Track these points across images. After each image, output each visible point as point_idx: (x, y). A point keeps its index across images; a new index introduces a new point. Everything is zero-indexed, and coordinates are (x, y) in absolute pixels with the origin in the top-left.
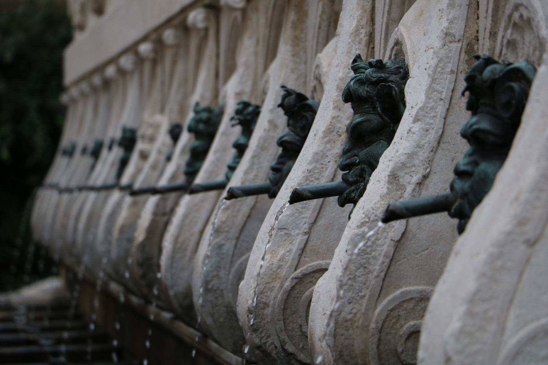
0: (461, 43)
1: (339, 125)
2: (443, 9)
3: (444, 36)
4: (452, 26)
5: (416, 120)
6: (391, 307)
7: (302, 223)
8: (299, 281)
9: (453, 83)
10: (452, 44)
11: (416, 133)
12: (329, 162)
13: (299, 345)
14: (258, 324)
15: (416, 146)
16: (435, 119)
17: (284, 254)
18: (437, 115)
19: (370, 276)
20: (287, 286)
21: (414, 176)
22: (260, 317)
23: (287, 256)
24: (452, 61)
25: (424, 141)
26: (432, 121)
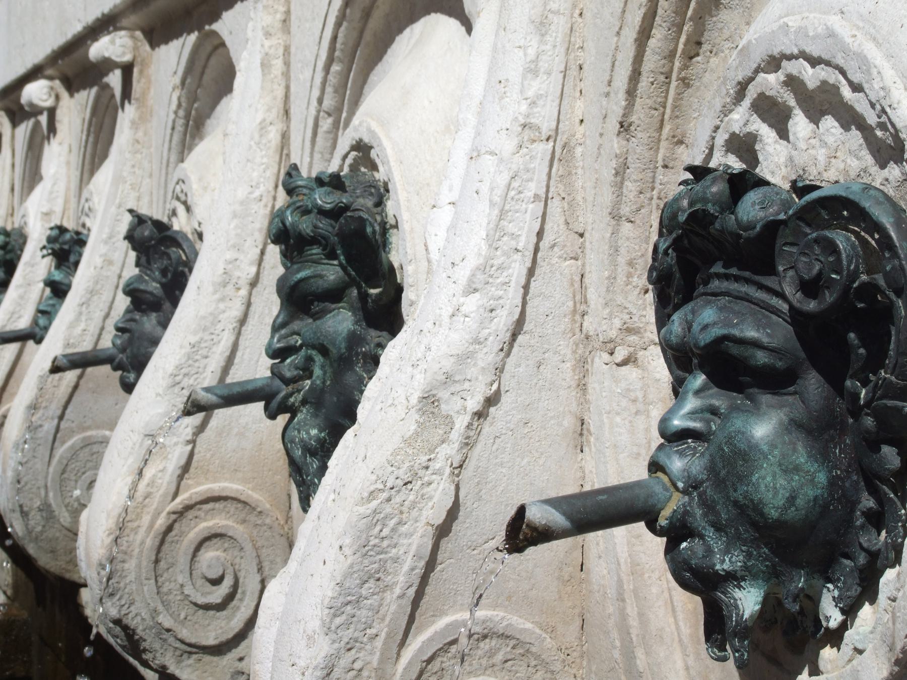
0: (551, 144)
1: (237, 273)
2: (507, 80)
3: (520, 129)
4: (535, 110)
5: (471, 290)
6: (430, 654)
7: (183, 426)
8: (179, 517)
9: (540, 219)
10: (535, 144)
11: (472, 315)
12: (223, 330)
13: (179, 615)
14: (115, 585)
15: (471, 341)
16: (508, 288)
17: (154, 475)
18: (510, 280)
19: (388, 595)
20: (161, 525)
21: (468, 398)
22: (118, 574)
23: (160, 478)
24: (535, 178)
25: (487, 331)
26: (501, 293)
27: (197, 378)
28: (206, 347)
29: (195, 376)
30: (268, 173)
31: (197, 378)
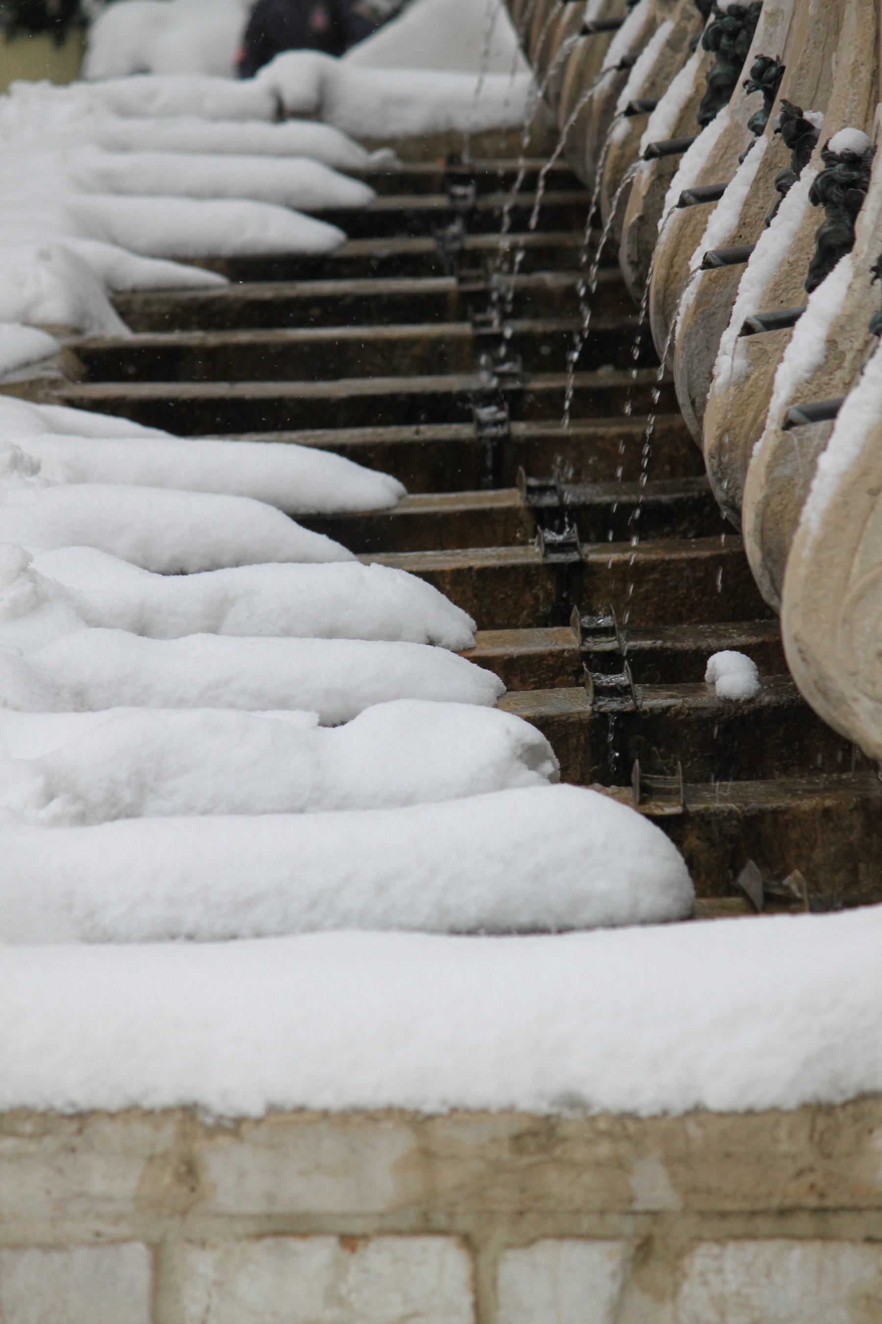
7: (782, 334)
17: (757, 377)
23: (762, 380)
27: (795, 292)
28: (803, 265)
29: (793, 291)
30: (859, 109)
31: (795, 292)
